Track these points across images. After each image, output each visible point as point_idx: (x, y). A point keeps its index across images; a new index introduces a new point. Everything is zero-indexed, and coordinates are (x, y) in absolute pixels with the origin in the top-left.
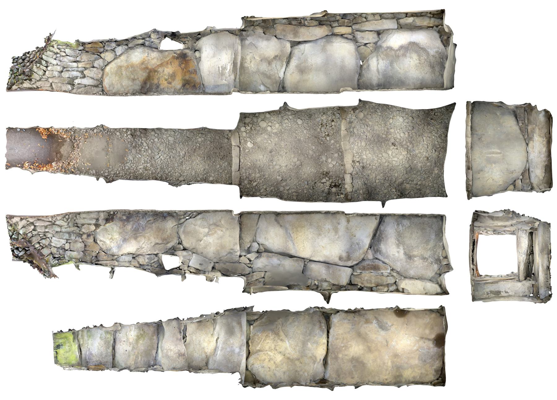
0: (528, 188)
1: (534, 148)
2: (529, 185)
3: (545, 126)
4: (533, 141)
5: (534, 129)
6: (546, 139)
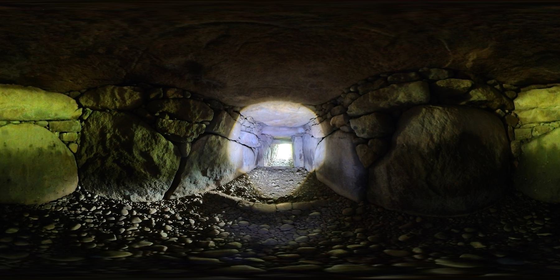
1: (15, 109)
2: (74, 122)
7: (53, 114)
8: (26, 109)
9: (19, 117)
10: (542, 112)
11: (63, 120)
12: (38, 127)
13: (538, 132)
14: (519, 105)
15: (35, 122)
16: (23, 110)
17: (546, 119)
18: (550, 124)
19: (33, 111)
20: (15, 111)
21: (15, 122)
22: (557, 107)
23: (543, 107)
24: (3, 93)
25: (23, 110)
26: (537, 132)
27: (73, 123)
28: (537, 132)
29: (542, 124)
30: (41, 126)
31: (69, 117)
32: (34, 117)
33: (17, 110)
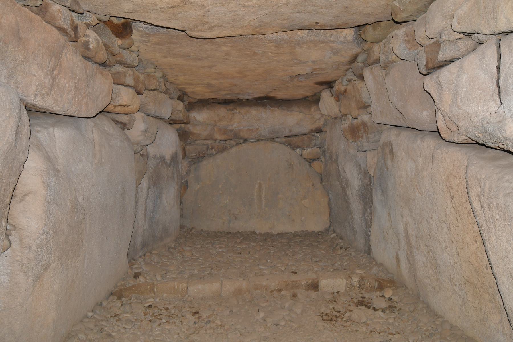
0: (318, 137)
1: (251, 128)
2: (314, 136)
3: (216, 111)
4: (240, 130)
5: (220, 130)
6: (236, 109)
7: (287, 130)
8: (260, 129)
9: (255, 136)
10: (220, 130)
11: (297, 136)
12: (276, 145)
13: (215, 150)
14: (196, 120)
15: (273, 140)
16: (258, 129)
17: (223, 137)
18: (227, 142)
19: (267, 130)
20: (250, 130)
21: (252, 140)
22: (234, 126)
23: (221, 126)
24: (239, 112)
25: (258, 129)
26: (213, 150)
27: (312, 137)
28: (213, 150)
29: (217, 141)
30: (280, 143)
31: (306, 131)
32: (268, 136)
33: (252, 130)
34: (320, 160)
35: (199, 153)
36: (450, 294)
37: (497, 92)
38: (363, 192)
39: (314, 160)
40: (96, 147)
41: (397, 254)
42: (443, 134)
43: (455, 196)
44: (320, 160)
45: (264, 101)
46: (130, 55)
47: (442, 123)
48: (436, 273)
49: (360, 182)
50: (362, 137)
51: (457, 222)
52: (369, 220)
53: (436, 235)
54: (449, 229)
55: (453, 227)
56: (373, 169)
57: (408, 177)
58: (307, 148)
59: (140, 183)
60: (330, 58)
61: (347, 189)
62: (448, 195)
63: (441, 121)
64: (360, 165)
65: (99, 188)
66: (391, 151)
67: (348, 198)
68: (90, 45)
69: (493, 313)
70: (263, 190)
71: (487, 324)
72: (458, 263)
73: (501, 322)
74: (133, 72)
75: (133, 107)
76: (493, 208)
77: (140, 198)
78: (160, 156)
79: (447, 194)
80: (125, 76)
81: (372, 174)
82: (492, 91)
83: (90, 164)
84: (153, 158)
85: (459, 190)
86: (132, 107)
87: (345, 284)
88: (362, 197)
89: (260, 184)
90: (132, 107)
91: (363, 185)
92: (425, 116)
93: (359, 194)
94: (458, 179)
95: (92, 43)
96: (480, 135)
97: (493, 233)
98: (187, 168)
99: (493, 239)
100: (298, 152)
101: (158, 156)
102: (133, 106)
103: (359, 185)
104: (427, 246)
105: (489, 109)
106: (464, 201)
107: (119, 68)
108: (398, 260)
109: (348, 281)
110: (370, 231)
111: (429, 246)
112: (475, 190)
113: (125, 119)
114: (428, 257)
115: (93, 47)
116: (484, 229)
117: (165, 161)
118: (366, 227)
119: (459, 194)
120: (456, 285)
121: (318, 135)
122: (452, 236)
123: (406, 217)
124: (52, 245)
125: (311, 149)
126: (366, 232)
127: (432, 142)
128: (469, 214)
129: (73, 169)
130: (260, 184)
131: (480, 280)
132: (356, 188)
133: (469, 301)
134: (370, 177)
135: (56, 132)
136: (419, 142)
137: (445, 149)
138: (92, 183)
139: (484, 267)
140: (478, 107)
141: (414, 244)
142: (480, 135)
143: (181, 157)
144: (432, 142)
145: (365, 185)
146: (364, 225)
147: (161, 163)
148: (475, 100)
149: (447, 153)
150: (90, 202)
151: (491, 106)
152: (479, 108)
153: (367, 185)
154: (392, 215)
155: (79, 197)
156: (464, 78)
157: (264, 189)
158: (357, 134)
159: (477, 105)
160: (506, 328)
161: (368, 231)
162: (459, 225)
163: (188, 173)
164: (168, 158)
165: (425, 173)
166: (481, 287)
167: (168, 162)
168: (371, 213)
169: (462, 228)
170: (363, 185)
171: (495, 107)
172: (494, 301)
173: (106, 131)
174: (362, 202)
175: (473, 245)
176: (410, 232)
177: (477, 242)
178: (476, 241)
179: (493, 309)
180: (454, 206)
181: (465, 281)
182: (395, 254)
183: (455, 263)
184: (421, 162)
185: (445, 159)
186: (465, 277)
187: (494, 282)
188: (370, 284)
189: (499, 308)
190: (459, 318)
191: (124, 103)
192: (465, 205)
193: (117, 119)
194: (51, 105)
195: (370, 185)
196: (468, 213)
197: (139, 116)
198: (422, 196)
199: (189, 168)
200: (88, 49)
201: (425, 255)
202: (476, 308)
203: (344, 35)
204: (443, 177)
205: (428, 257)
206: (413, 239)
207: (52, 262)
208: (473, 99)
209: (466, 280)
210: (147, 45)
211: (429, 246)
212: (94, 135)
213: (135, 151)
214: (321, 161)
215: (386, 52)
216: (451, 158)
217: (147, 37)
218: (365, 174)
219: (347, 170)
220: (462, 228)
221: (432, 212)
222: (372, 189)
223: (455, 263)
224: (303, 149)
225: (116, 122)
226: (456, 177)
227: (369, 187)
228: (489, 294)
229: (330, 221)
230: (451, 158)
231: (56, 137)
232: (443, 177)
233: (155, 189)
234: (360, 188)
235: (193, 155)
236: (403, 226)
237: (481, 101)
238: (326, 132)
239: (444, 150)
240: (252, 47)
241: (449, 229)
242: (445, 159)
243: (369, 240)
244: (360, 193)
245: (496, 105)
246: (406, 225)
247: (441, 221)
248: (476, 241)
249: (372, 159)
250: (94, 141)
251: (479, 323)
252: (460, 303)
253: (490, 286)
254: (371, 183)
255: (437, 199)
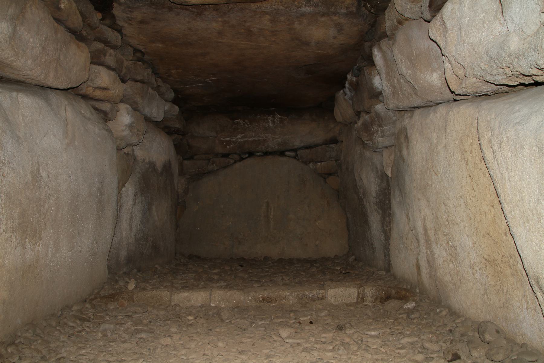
13: (216, 165)
15: (282, 154)
26: (214, 165)
28: (214, 165)
34: (336, 175)
35: (199, 169)
36: (472, 285)
37: (500, 10)
38: (381, 198)
39: (330, 174)
40: (68, 127)
41: (417, 260)
42: (451, 86)
43: (470, 159)
44: (336, 175)
45: (272, 109)
46: (112, 33)
47: (450, 73)
48: (456, 265)
49: (378, 187)
50: (377, 131)
51: (473, 191)
52: (388, 231)
53: (454, 217)
54: (466, 203)
55: (470, 199)
56: (391, 168)
57: (424, 160)
58: (321, 162)
59: (123, 186)
60: (335, 38)
61: (364, 200)
62: (463, 161)
63: (449, 71)
64: (377, 168)
65: (70, 172)
66: (406, 137)
67: (365, 210)
68: (61, 4)
69: (515, 289)
70: (271, 209)
71: (510, 306)
72: (477, 243)
73: (525, 296)
74: (115, 53)
75: (115, 93)
76: (503, 145)
77: (124, 205)
78: (149, 161)
79: (461, 161)
80: (105, 55)
81: (389, 175)
82: (495, 10)
83: (59, 143)
84: (142, 163)
85: (473, 151)
86: (114, 92)
87: (356, 294)
88: (379, 204)
89: (268, 203)
90: (114, 92)
91: (381, 190)
92: (436, 80)
93: (376, 202)
94: (471, 138)
95: (63, 2)
96: (486, 67)
97: (507, 179)
98: (184, 186)
99: (507, 186)
100: (311, 167)
101: (147, 161)
102: (114, 91)
103: (376, 191)
104: (446, 235)
105: (493, 31)
106: (478, 162)
107: (100, 46)
108: (418, 267)
109: (359, 291)
110: (389, 245)
111: (448, 235)
112: (486, 137)
113: (106, 107)
114: (448, 249)
115: (64, 6)
116: (498, 180)
117: (156, 168)
118: (386, 240)
119: (473, 155)
120: (476, 271)
121: (333, 146)
122: (469, 211)
123: (424, 210)
124: (4, 211)
125: (325, 162)
126: (385, 246)
127: (444, 109)
128: (484, 176)
129: (38, 141)
130: (268, 203)
131: (500, 253)
132: (373, 194)
133: (491, 284)
134: (388, 180)
135: (20, 97)
136: (432, 115)
137: (456, 109)
138: (61, 163)
139: (503, 234)
140: (482, 33)
141: (433, 240)
142: (486, 67)
143: (178, 171)
144: (444, 109)
145: (382, 189)
146: (383, 237)
147: (150, 170)
148: (478, 26)
149: (458, 113)
150: (58, 183)
151: (495, 28)
152: (483, 34)
153: (385, 189)
154: (410, 216)
155: (43, 172)
156: (467, 5)
157: (272, 209)
158: (371, 130)
159: (481, 30)
160: (530, 302)
161: (388, 244)
162: (476, 194)
163: (186, 191)
164: (159, 166)
165: (439, 147)
166: (502, 261)
167: (160, 169)
168: (390, 223)
169: (479, 196)
170: (381, 190)
171: (499, 28)
172: (515, 274)
173: (83, 114)
174: (380, 211)
175: (491, 211)
176: (429, 226)
177: (495, 207)
178: (493, 206)
179: (515, 284)
180: (469, 172)
181: (485, 262)
182: (416, 261)
183: (474, 243)
184: (435, 137)
185: (457, 120)
186: (485, 256)
187: (514, 248)
188: (385, 293)
189: (521, 280)
190: (482, 312)
191: (103, 85)
192: (479, 167)
193: (97, 106)
194: (11, 57)
195: (389, 189)
196: (483, 175)
197: (123, 108)
198: (438, 176)
199: (187, 187)
200: (59, 9)
201: (444, 247)
202: (498, 290)
203: (346, 6)
204: (457, 143)
205: (448, 249)
206: (431, 233)
207: (4, 231)
208: (476, 25)
209: (486, 260)
210: (132, 25)
211: (448, 235)
212: (67, 114)
213: (118, 147)
214: (338, 176)
215: (391, 16)
216: (463, 117)
217: (130, 11)
218: (383, 176)
219: (364, 177)
220: (479, 196)
221: (448, 192)
222: (390, 193)
223: (474, 243)
224: (317, 162)
225: (96, 109)
226: (468, 136)
227: (386, 191)
228: (511, 268)
229: (349, 246)
230: (463, 117)
231: (20, 103)
232: (457, 143)
233: (143, 198)
234: (378, 193)
235: (192, 171)
236: (422, 222)
237: (485, 25)
238: (342, 142)
239: (455, 110)
240: (245, 22)
241: (466, 203)
242: (457, 120)
243: (389, 255)
244: (378, 200)
245: (500, 25)
246: (425, 219)
247: (458, 198)
248: (493, 206)
249: (389, 157)
250: (66, 120)
251: (502, 308)
252: (482, 293)
253: (510, 256)
254: (389, 186)
255: (452, 173)
